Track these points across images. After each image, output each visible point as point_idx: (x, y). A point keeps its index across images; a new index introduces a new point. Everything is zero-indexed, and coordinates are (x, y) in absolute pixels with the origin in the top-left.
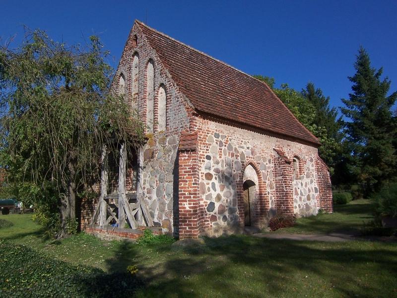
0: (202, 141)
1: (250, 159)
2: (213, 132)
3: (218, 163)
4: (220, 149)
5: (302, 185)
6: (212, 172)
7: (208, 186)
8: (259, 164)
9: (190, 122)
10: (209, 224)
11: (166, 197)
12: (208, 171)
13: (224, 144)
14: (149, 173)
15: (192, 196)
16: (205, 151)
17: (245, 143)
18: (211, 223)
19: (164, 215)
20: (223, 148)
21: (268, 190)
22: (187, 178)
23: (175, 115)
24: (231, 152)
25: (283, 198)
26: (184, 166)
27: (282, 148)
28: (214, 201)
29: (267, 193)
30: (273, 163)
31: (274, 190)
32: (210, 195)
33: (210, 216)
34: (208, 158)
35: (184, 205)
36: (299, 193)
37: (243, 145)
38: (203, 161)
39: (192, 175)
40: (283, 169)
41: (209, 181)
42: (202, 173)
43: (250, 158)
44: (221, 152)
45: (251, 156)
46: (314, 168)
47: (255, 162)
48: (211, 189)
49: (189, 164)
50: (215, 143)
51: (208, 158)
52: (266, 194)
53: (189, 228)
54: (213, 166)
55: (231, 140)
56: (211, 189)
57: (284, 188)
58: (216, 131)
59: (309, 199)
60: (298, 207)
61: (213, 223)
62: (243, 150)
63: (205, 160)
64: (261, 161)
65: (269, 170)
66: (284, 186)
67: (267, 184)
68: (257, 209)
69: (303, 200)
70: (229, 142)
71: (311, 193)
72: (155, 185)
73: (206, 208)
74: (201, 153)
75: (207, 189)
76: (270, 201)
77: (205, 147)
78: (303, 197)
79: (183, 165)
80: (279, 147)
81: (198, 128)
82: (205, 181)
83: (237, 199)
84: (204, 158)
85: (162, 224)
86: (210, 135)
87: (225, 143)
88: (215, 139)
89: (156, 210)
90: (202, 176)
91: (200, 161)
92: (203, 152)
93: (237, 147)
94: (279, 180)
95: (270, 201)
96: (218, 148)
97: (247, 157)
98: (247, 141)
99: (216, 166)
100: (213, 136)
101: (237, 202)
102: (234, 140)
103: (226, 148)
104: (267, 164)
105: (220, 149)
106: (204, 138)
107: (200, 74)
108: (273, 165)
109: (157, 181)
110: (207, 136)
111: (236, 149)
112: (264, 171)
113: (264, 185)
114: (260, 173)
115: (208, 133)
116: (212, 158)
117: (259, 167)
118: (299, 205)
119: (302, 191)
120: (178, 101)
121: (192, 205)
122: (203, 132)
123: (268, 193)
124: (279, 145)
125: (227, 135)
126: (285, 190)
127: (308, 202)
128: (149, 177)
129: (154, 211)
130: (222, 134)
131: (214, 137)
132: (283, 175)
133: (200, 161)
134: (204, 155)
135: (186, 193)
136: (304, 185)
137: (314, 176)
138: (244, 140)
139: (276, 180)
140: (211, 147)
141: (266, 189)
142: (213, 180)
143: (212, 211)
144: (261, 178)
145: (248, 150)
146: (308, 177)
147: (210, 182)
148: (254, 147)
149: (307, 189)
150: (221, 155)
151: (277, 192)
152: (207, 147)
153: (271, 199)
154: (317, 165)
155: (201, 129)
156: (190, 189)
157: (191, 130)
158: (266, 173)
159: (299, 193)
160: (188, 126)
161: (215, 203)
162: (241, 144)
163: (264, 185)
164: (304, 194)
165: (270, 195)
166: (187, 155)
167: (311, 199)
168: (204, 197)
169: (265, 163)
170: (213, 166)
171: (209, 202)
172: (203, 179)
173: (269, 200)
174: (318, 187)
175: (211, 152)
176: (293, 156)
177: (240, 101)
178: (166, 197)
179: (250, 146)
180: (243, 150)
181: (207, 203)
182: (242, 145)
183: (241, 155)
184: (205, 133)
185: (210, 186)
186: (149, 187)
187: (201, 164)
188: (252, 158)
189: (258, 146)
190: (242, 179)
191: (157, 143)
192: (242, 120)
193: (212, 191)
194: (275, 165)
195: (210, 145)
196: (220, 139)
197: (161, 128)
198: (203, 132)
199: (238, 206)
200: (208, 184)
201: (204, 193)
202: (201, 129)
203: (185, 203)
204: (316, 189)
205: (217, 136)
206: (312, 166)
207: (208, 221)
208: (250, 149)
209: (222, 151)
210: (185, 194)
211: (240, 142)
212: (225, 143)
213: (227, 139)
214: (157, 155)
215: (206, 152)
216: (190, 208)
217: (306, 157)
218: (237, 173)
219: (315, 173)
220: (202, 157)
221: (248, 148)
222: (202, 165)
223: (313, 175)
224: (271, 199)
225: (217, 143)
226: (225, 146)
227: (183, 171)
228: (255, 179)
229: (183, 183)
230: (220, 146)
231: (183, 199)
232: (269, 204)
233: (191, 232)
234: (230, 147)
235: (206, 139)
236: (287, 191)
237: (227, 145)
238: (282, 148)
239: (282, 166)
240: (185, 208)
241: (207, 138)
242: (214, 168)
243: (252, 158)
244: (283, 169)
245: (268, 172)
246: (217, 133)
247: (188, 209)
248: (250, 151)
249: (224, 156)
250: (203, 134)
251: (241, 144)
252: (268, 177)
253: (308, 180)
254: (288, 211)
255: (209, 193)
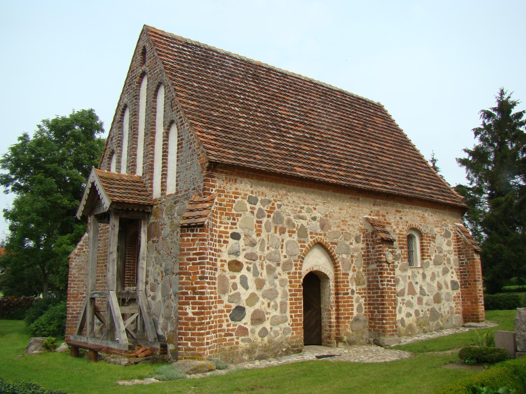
0: (225, 210)
1: (317, 237)
2: (246, 195)
3: (253, 244)
4: (257, 222)
5: (424, 276)
6: (241, 259)
7: (233, 280)
8: (336, 244)
9: (205, 180)
10: (233, 340)
11: (173, 297)
12: (233, 258)
13: (267, 213)
14: (153, 260)
15: (197, 296)
16: (230, 225)
17: (309, 211)
18: (238, 338)
19: (169, 325)
20: (265, 220)
21: (353, 286)
22: (190, 268)
23: (187, 169)
24: (281, 225)
25: (378, 300)
26: (188, 250)
27: (383, 216)
28: (243, 304)
29: (349, 291)
30: (363, 241)
31: (365, 286)
32: (238, 296)
33: (237, 327)
34: (236, 236)
35: (186, 309)
36: (418, 290)
37: (304, 213)
38: (225, 242)
39: (199, 264)
40: (378, 251)
41: (235, 274)
42: (222, 261)
43: (317, 234)
44: (260, 226)
45: (319, 231)
46: (452, 248)
47: (326, 240)
48: (239, 286)
49: (195, 247)
50: (248, 213)
51: (236, 236)
52: (348, 294)
53: (191, 344)
54: (244, 250)
55: (279, 206)
56: (239, 286)
57: (380, 283)
58: (252, 192)
59: (437, 299)
60: (413, 314)
61: (240, 338)
62: (304, 222)
63: (230, 240)
64: (340, 239)
65: (356, 254)
66: (379, 279)
67: (349, 277)
68: (331, 318)
69: (424, 302)
70: (277, 209)
71: (444, 291)
72: (159, 279)
73: (228, 314)
74: (222, 229)
75: (231, 285)
76: (356, 305)
77: (229, 219)
78: (425, 299)
79: (186, 248)
80: (377, 215)
81: (218, 191)
82: (228, 274)
83: (288, 302)
84: (226, 237)
85: (167, 338)
86: (239, 199)
87: (268, 212)
88: (249, 206)
89: (161, 316)
90: (222, 266)
91: (219, 241)
92: (226, 228)
93: (292, 218)
94: (373, 270)
95: (356, 305)
96: (255, 221)
97: (311, 233)
98: (311, 207)
99: (249, 250)
100: (246, 201)
101: (289, 306)
102: (285, 207)
103: (270, 220)
104: (351, 244)
105: (257, 222)
106: (228, 205)
107: (243, 99)
108: (364, 246)
109: (162, 272)
110: (234, 202)
111: (289, 221)
112: (344, 256)
113: (343, 278)
114: (337, 259)
115: (236, 198)
116: (243, 237)
117: (335, 250)
118: (417, 312)
119: (425, 288)
120: (190, 148)
121: (197, 310)
122: (226, 196)
123: (353, 292)
124: (378, 212)
125: (272, 199)
126: (381, 287)
127: (436, 306)
128: (153, 266)
129: (158, 318)
130: (263, 198)
131: (248, 204)
132: (379, 262)
133: (219, 241)
134: (227, 233)
135: (189, 292)
136: (428, 279)
137: (452, 262)
138: (306, 206)
139: (368, 270)
140: (240, 219)
141: (348, 286)
142: (244, 272)
143: (240, 320)
144: (339, 266)
145: (314, 222)
146: (437, 263)
147: (238, 275)
148: (326, 216)
149: (435, 285)
150: (261, 231)
151: (369, 289)
152: (234, 219)
153: (357, 301)
154: (458, 242)
155: (223, 192)
156: (195, 285)
157: (204, 194)
158: (349, 258)
159: (418, 290)
160: (202, 188)
161: (247, 307)
162: (300, 212)
163: (343, 278)
164: (427, 293)
165: (356, 295)
166: (192, 234)
167: (443, 301)
168: (225, 298)
169: (348, 243)
170: (244, 250)
171: (234, 306)
172: (224, 271)
173: (354, 303)
174: (458, 281)
175: (241, 228)
176: (406, 228)
177: (313, 139)
178: (173, 297)
179: (318, 215)
180: (304, 222)
181: (230, 307)
182: (301, 214)
183: (299, 230)
184: (231, 197)
185: (237, 281)
186: (153, 281)
187: (221, 246)
188: (321, 234)
189: (335, 215)
190: (300, 269)
191: (164, 213)
192: (301, 172)
193: (240, 289)
194: (367, 244)
195: (239, 215)
196: (258, 206)
197: (171, 189)
198: (226, 196)
199: (291, 312)
200: (234, 277)
201: (224, 292)
202: (223, 192)
203: (187, 307)
204: (453, 283)
205: (253, 201)
206: (448, 244)
207: (231, 335)
208: (318, 219)
209: (263, 225)
210: (187, 293)
211: (299, 209)
212: (268, 212)
213: (273, 204)
214: (163, 232)
215: (231, 228)
216: (194, 314)
217: (436, 230)
218: (290, 260)
219: (453, 257)
220: (224, 235)
221: (314, 219)
222: (223, 249)
223: (449, 260)
224: (357, 301)
225: (252, 213)
226: (269, 216)
227: (185, 257)
228: (327, 268)
229: (184, 276)
230: (258, 217)
231: (184, 300)
232: (352, 310)
233: (194, 349)
234: (278, 219)
235: (232, 206)
236: (383, 289)
237: (272, 215)
238: (383, 216)
239: (377, 246)
240: (187, 314)
241: (234, 205)
242: (245, 252)
243: (321, 234)
244: (378, 251)
245: (352, 256)
246: (254, 196)
247: (191, 315)
248: (318, 224)
249: (266, 234)
250: (227, 199)
251: (300, 212)
252: (353, 265)
253: (439, 269)
254: (384, 321)
255: (236, 292)
